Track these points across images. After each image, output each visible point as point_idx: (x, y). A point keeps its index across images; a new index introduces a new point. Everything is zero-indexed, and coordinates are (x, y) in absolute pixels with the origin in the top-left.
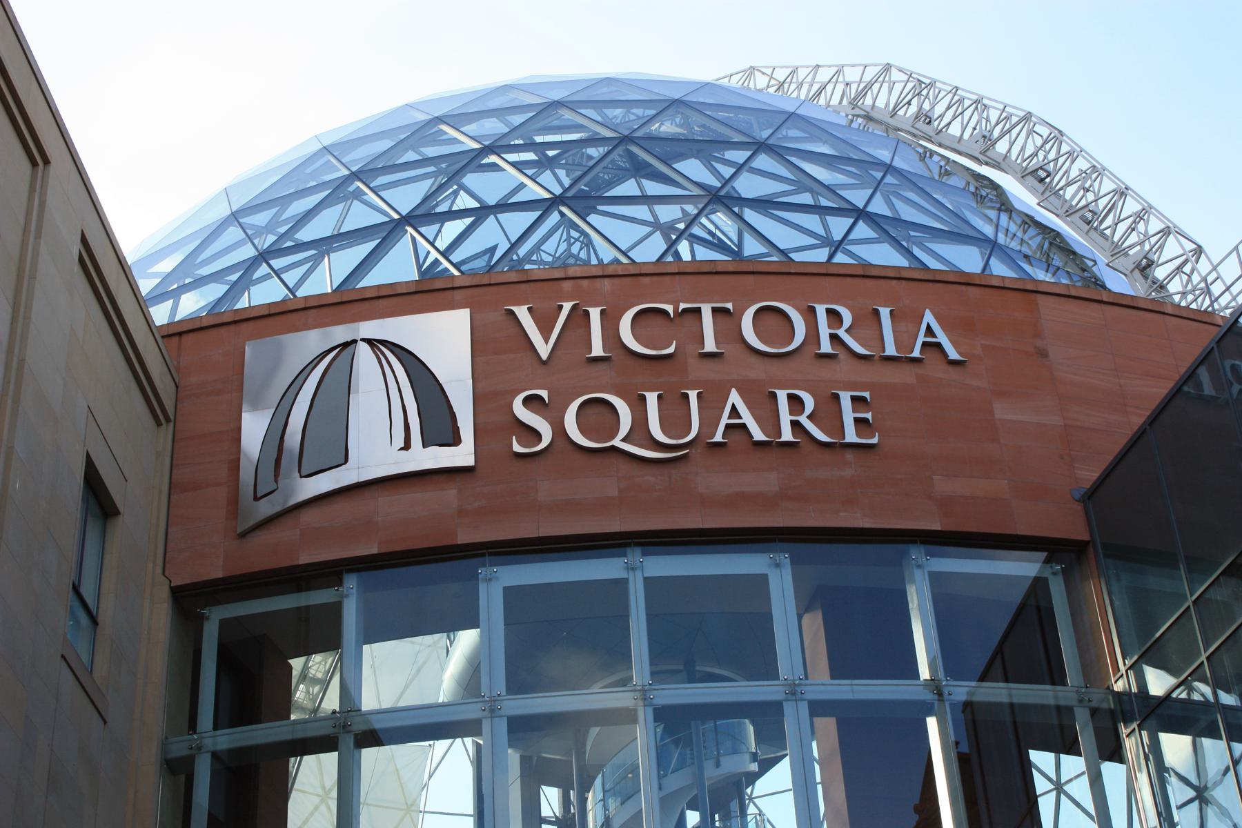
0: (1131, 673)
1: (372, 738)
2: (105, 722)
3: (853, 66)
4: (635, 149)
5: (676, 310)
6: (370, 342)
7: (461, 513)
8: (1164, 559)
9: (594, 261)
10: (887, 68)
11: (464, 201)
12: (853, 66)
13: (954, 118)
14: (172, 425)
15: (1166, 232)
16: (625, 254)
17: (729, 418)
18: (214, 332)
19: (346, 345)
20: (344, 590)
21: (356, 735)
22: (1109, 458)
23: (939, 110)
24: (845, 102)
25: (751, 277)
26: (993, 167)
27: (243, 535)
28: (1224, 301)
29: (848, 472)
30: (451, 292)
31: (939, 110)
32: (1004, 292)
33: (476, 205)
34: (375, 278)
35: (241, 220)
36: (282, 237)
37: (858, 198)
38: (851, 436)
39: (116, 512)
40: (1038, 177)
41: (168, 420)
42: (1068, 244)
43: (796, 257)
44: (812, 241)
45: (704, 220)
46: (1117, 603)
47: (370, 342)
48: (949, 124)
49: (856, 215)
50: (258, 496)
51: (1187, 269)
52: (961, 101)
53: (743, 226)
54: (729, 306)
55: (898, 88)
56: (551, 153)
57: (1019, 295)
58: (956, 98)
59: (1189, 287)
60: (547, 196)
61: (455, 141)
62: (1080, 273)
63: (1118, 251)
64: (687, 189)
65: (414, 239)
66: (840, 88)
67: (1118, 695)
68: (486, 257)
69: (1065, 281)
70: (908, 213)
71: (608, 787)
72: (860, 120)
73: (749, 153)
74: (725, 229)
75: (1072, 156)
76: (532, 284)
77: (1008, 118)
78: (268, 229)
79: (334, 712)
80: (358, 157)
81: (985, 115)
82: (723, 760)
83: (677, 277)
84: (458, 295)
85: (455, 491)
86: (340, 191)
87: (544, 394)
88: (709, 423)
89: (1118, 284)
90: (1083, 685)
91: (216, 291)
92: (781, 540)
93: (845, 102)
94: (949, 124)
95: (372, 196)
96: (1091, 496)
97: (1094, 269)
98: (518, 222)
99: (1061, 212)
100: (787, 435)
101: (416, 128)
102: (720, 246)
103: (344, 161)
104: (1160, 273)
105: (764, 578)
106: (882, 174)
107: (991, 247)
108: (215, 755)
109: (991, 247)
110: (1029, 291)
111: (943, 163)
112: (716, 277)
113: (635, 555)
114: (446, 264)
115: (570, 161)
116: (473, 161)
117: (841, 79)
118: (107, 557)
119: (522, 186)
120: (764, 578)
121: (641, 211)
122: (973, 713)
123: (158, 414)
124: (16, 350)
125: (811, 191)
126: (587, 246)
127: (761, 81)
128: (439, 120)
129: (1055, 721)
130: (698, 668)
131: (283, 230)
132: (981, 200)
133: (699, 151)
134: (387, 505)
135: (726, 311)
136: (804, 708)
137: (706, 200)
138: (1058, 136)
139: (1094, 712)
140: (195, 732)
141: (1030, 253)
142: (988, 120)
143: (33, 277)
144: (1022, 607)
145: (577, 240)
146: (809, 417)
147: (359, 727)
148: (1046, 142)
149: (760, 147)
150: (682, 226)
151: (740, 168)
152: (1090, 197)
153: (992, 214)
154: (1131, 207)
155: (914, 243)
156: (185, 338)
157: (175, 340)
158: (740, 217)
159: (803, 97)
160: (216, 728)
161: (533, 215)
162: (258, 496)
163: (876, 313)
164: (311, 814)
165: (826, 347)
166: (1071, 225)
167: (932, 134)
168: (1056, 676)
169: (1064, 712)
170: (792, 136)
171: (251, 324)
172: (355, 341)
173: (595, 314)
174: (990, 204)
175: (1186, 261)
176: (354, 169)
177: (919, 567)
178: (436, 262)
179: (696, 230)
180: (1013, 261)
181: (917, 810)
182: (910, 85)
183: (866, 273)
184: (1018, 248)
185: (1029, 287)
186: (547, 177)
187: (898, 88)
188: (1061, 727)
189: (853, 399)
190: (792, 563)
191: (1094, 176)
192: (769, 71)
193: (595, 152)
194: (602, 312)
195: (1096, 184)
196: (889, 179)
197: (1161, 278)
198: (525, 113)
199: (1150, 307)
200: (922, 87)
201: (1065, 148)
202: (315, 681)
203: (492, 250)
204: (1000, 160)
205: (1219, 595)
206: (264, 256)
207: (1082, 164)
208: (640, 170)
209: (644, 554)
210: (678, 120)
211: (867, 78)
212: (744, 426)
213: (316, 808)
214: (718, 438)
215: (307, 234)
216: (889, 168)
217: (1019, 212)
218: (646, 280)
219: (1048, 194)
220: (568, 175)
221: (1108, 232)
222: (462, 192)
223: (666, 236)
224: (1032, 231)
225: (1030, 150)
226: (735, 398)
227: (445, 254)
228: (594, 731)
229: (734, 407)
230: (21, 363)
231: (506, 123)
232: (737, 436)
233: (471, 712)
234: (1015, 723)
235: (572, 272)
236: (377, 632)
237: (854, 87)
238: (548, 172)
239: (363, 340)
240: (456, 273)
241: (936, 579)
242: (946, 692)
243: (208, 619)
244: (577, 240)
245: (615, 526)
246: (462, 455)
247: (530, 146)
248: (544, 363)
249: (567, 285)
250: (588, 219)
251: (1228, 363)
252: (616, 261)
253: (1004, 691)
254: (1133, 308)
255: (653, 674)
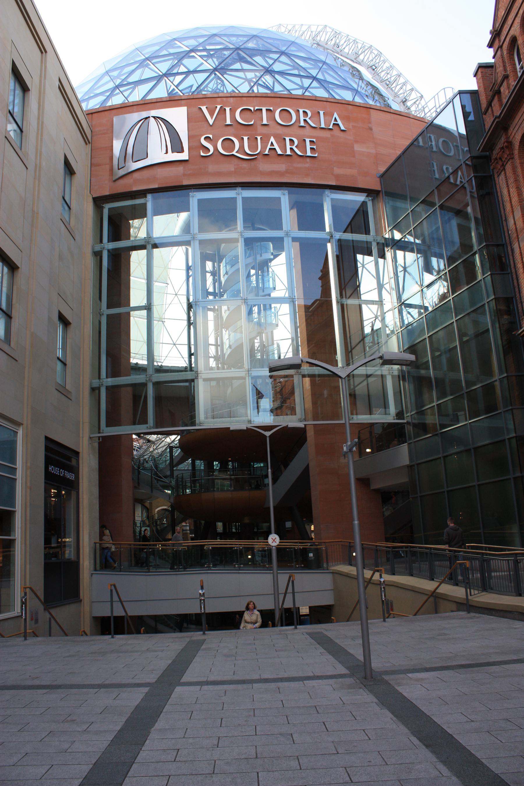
0: (390, 232)
1: (155, 246)
2: (75, 240)
3: (314, 25)
4: (240, 52)
5: (254, 110)
6: (154, 117)
7: (184, 175)
8: (403, 197)
9: (225, 92)
10: (326, 26)
11: (182, 69)
12: (314, 25)
13: (346, 46)
14: (90, 144)
15: (412, 90)
16: (236, 88)
17: (270, 146)
18: (103, 113)
19: (146, 118)
20: (147, 199)
21: (152, 245)
22: (388, 164)
23: (341, 43)
24: (311, 38)
25: (279, 99)
26: (358, 64)
27: (115, 181)
28: (428, 115)
29: (307, 165)
30: (180, 101)
31: (341, 43)
32: (360, 107)
33: (186, 70)
34: (153, 96)
35: (109, 74)
36: (123, 80)
37: (314, 72)
38: (309, 154)
39: (75, 173)
40: (373, 68)
41: (89, 143)
42: (380, 92)
43: (293, 92)
44: (297, 87)
45: (262, 79)
46: (388, 210)
47: (154, 117)
48: (344, 48)
49: (313, 79)
50: (119, 168)
51: (417, 103)
52: (349, 40)
53: (275, 80)
54: (272, 108)
55: (329, 34)
56: (212, 53)
57: (364, 109)
58: (348, 39)
59: (418, 109)
60: (212, 68)
61: (180, 47)
62: (383, 102)
63: (396, 95)
64: (257, 67)
65: (165, 81)
66: (309, 33)
67: (385, 239)
68: (190, 89)
69: (378, 105)
70: (329, 79)
71: (227, 262)
72: (315, 45)
73: (278, 55)
74: (269, 81)
75: (384, 62)
76: (207, 99)
77: (364, 47)
78: (118, 77)
79: (145, 238)
80: (148, 52)
81: (357, 45)
82: (262, 255)
83: (255, 98)
84: (183, 102)
85: (182, 168)
86: (142, 64)
87: (211, 136)
88: (264, 147)
89: (396, 106)
90: (375, 235)
91: (102, 98)
92: (285, 187)
93: (311, 38)
94: (344, 48)
95: (152, 66)
96: (382, 176)
97: (388, 101)
98: (200, 77)
99: (379, 81)
100: (289, 152)
101: (167, 42)
102: (267, 88)
103: (143, 53)
104: (409, 104)
105: (280, 198)
106: (322, 65)
107: (356, 92)
108: (108, 251)
109: (356, 92)
110: (368, 108)
111: (342, 62)
112: (268, 99)
113: (239, 190)
114: (177, 90)
115: (218, 56)
116: (187, 54)
117: (310, 30)
118: (72, 188)
119: (202, 64)
120: (280, 198)
121: (241, 74)
122: (341, 242)
123: (86, 141)
124: (41, 119)
125: (298, 69)
126: (223, 86)
127: (283, 29)
128: (175, 39)
129: (366, 246)
130: (256, 226)
131: (123, 78)
132: (353, 75)
133: (261, 54)
134: (161, 172)
135: (270, 110)
136: (290, 239)
137: (264, 71)
138: (380, 54)
139: (378, 244)
140: (102, 243)
141: (368, 95)
142: (357, 47)
143: (44, 93)
144: (358, 211)
145: (220, 83)
146: (296, 147)
147: (152, 243)
148: (376, 56)
149: (282, 53)
150: (254, 80)
151: (275, 60)
152: (389, 76)
153: (357, 80)
154: (402, 80)
155: (331, 89)
156: (94, 115)
157: (90, 115)
158: (274, 77)
159: (297, 36)
160: (108, 242)
161: (207, 74)
162: (119, 168)
163: (319, 113)
164: (136, 269)
165: (302, 123)
166: (382, 86)
167: (339, 51)
168: (367, 232)
169: (368, 244)
170: (293, 50)
171: (115, 111)
172: (149, 117)
173: (228, 109)
174: (356, 77)
175: (418, 100)
176: (147, 56)
177: (328, 196)
178: (174, 90)
179: (260, 82)
180: (363, 97)
181: (322, 271)
182: (333, 33)
183: (316, 99)
184: (364, 93)
185: (368, 106)
186: (210, 61)
187: (329, 34)
188: (367, 247)
189: (310, 141)
190: (288, 194)
191: (391, 69)
192: (285, 26)
193: (227, 53)
194: (230, 109)
195: (391, 72)
196: (324, 67)
197: (409, 106)
198: (204, 38)
199: (406, 115)
200: (337, 34)
201: (382, 59)
202: (136, 228)
203: (191, 86)
204: (361, 62)
205: (418, 209)
206: (117, 87)
207: (387, 65)
208: (242, 59)
209: (242, 190)
210: (254, 42)
211: (318, 30)
212: (275, 149)
213: (137, 267)
214: (267, 152)
215: (131, 79)
216: (324, 63)
217: (366, 81)
218: (245, 99)
219: (375, 74)
220: (217, 61)
221: (393, 89)
222: (182, 66)
223: (250, 84)
224: (369, 87)
225: (370, 59)
226: (272, 139)
227: (177, 87)
228: (223, 245)
229: (272, 143)
230: (43, 122)
231: (197, 41)
232: (273, 152)
233: (187, 238)
234: (353, 246)
235: (220, 95)
236: (158, 212)
237: (314, 33)
238: (211, 59)
239: (152, 117)
240: (182, 94)
241: (332, 200)
242: (334, 236)
243: (105, 208)
244: (220, 83)
245: (233, 180)
246: (184, 156)
247: (205, 50)
248: (211, 126)
249: (219, 100)
250: (224, 76)
251: (428, 135)
252: (233, 91)
253: (350, 236)
254: (400, 115)
255: (244, 227)
